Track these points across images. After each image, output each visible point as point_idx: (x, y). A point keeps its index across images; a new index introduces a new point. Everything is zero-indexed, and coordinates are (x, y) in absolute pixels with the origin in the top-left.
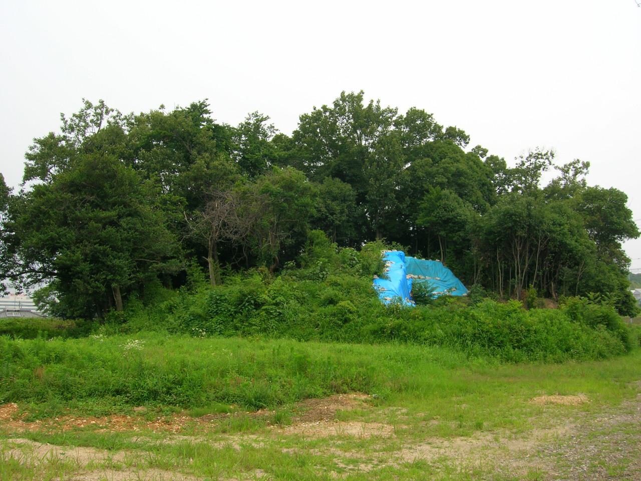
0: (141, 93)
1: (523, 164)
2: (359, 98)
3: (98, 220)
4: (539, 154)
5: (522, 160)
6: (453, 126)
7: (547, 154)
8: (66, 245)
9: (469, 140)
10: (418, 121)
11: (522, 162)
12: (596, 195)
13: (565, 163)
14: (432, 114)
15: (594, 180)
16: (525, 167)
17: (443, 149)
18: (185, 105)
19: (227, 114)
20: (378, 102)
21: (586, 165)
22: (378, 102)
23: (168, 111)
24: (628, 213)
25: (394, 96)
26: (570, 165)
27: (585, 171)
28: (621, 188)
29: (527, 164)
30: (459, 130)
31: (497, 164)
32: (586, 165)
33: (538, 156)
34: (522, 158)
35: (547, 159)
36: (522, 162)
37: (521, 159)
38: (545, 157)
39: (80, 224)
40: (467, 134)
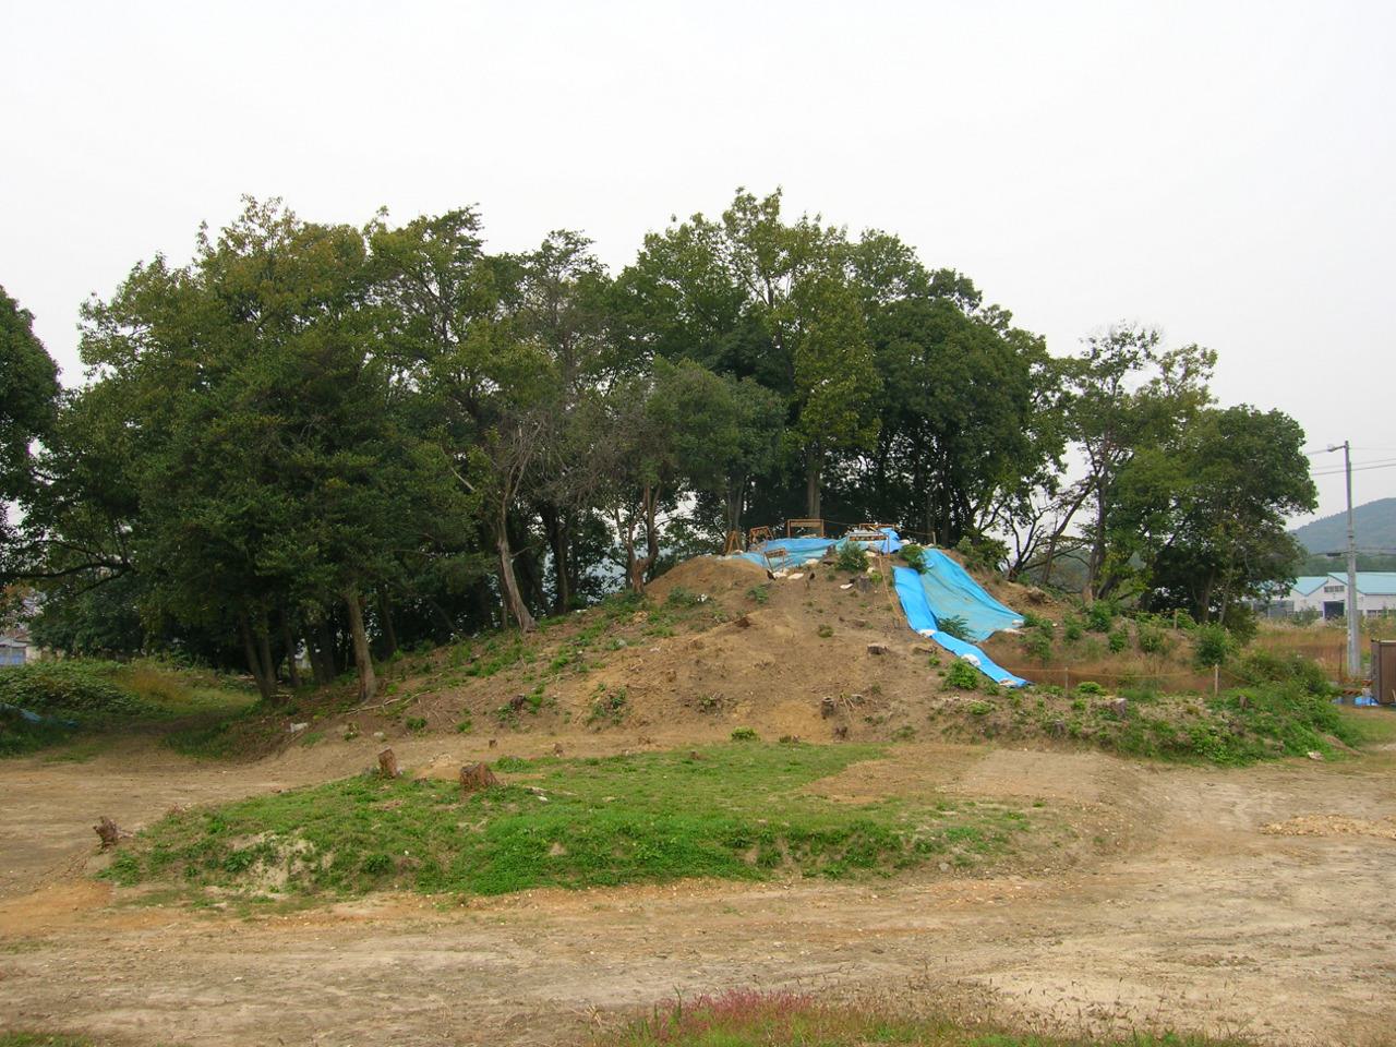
0: (356, 189)
1: (1096, 354)
2: (772, 204)
3: (339, 471)
4: (1126, 335)
5: (1095, 345)
6: (950, 270)
7: (1143, 336)
8: (280, 525)
9: (980, 299)
10: (883, 256)
11: (1094, 350)
12: (1240, 423)
13: (349, 223)
14: (914, 248)
15: (1227, 391)
16: (1100, 360)
17: (938, 320)
18: (437, 211)
19: (506, 235)
20: (818, 218)
21: (1211, 359)
22: (818, 218)
23: (397, 221)
24: (1303, 463)
25: (837, 202)
26: (1176, 354)
27: (1205, 370)
28: (1290, 411)
29: (1105, 356)
30: (961, 279)
31: (1037, 349)
32: (1211, 359)
33: (1122, 340)
34: (1094, 342)
35: (1144, 346)
36: (1094, 350)
37: (1092, 345)
38: (1139, 343)
39: (301, 482)
40: (976, 288)
